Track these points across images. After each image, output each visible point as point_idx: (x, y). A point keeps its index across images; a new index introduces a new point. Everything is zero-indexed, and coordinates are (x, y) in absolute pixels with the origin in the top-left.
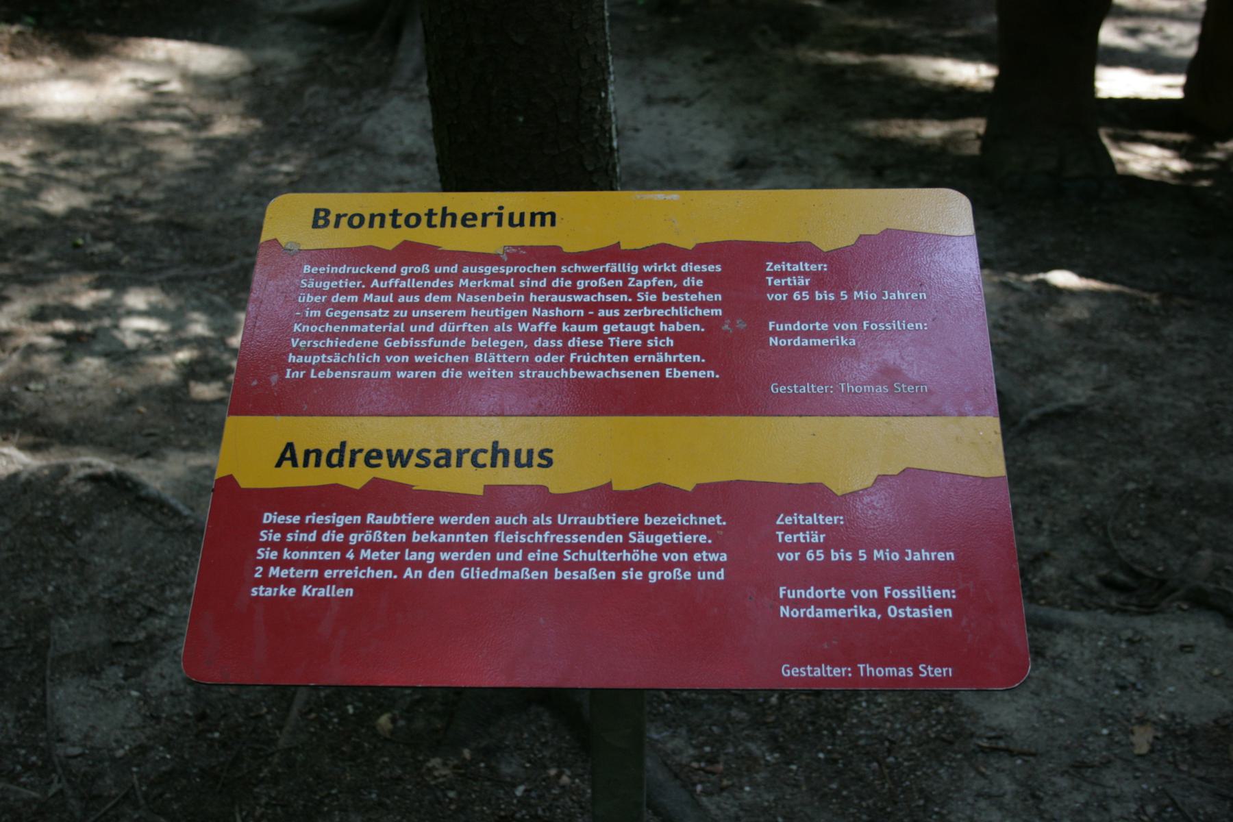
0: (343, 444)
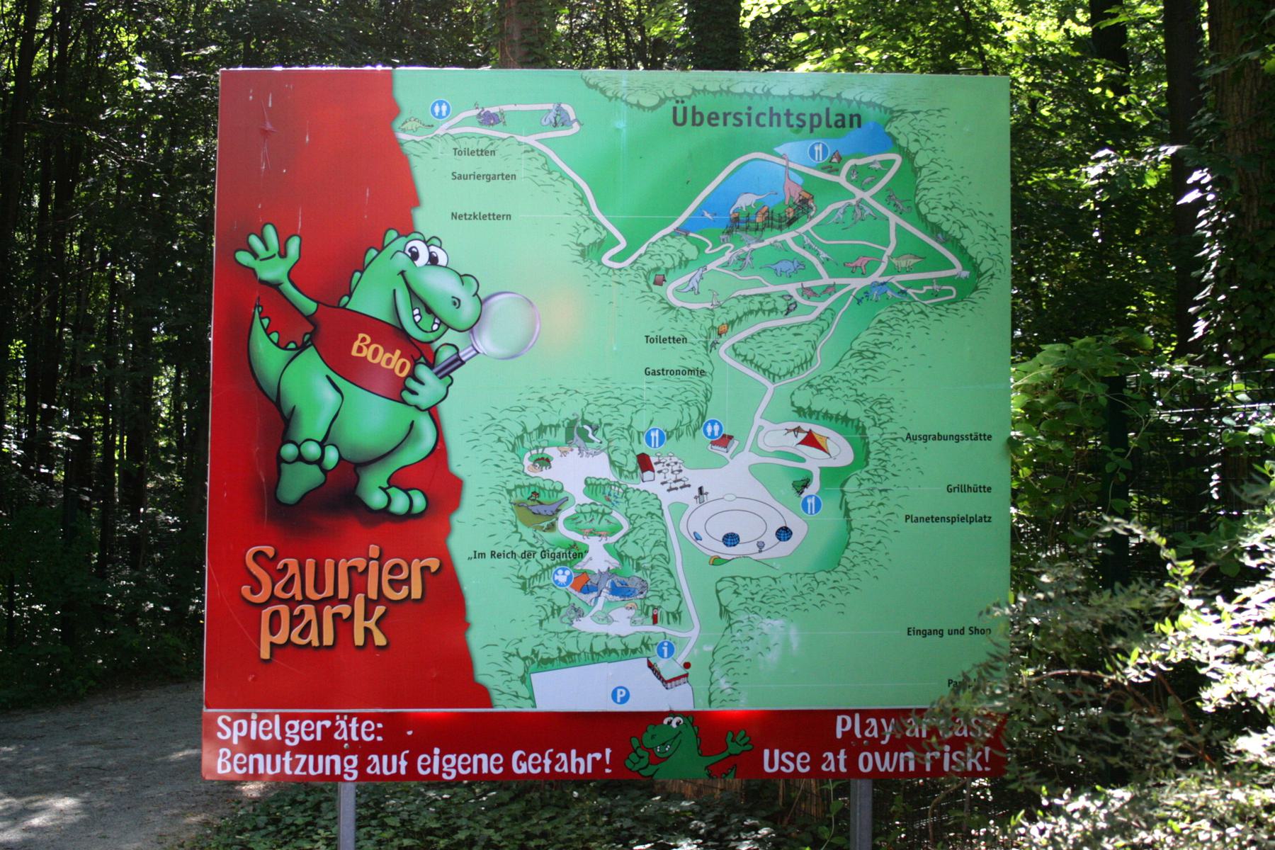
0: (812, 131)
